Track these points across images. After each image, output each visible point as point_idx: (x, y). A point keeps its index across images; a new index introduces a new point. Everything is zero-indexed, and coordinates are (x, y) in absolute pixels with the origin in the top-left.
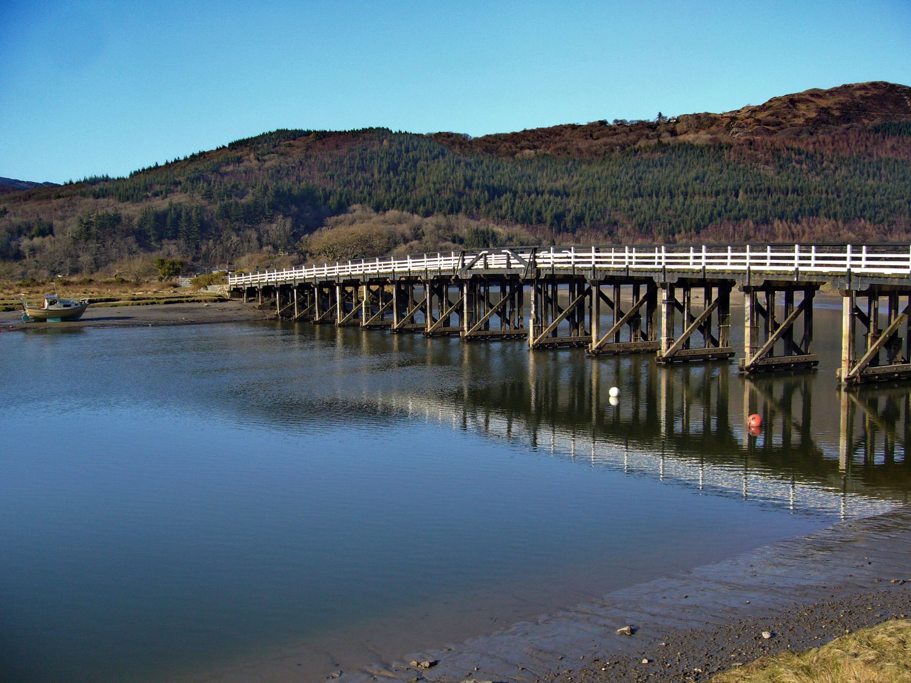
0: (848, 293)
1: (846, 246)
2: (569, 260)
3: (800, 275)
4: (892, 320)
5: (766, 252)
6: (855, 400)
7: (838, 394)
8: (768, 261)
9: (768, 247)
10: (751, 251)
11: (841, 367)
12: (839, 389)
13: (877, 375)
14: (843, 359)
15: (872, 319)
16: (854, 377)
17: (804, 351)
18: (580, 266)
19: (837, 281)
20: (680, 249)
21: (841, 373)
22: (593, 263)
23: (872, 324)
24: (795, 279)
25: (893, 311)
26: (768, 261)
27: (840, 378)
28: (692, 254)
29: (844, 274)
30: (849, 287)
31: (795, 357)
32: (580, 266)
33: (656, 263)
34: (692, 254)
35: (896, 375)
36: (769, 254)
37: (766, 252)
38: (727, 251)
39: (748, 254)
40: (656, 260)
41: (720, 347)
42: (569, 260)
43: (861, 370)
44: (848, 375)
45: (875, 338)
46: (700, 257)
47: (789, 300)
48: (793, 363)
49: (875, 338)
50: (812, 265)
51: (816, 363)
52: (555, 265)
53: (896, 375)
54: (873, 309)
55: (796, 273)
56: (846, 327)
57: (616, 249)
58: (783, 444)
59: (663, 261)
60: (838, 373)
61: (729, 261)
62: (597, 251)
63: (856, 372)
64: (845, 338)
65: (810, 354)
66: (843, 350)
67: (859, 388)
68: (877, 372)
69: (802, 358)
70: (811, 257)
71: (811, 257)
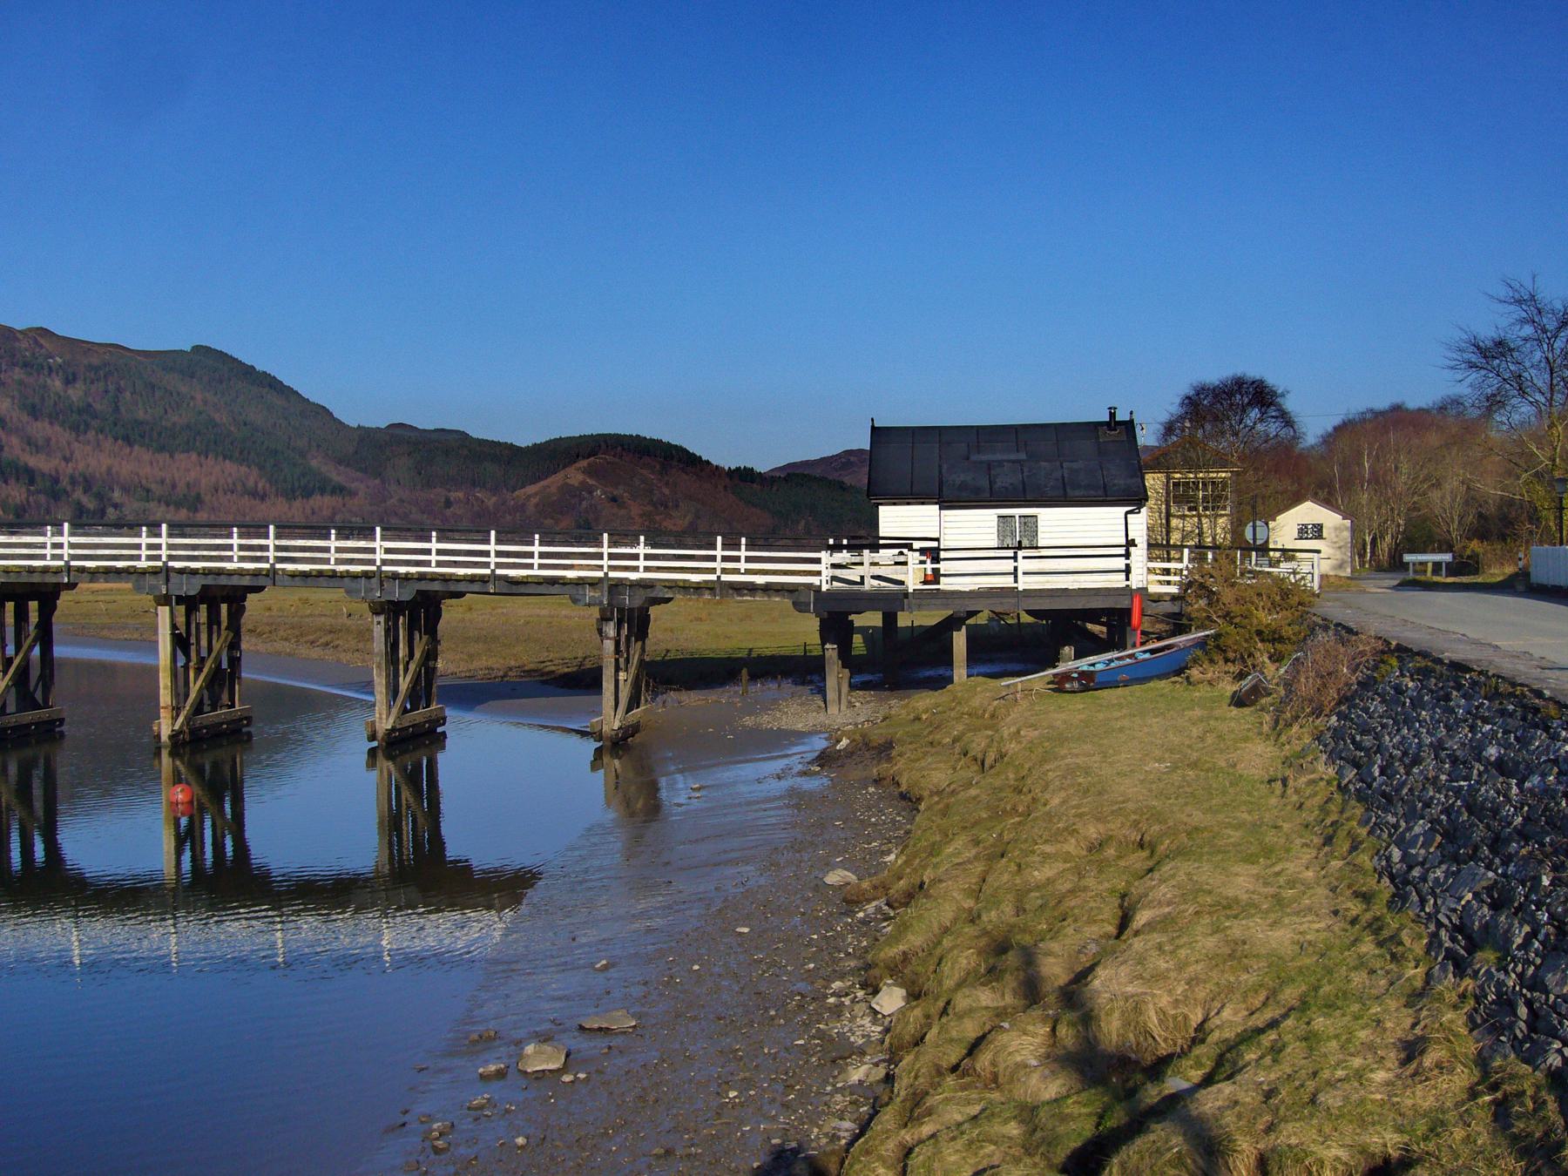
0: (165, 600)
1: (160, 526)
2: (325, 555)
3: (72, 573)
4: (214, 641)
5: (140, 536)
6: (182, 769)
7: (156, 762)
8: (641, 563)
9: (235, 530)
10: (499, 542)
11: (159, 718)
12: (158, 754)
13: (205, 727)
14: (162, 705)
15: (193, 640)
16: (180, 732)
17: (41, 702)
18: (290, 567)
19: (145, 581)
20: (558, 538)
21: (159, 728)
22: (164, 559)
23: (193, 648)
24: (66, 580)
25: (215, 627)
26: (641, 563)
27: (159, 736)
28: (144, 540)
29: (158, 570)
30: (167, 590)
31: (29, 716)
32: (290, 567)
33: (641, 569)
34: (144, 540)
35: (225, 726)
36: (235, 541)
37: (140, 536)
38: (487, 542)
39: (537, 548)
40: (48, 551)
41: (237, 708)
42: (325, 555)
43: (188, 719)
44: (173, 731)
45: (199, 670)
46: (158, 547)
47: (21, 616)
48: (33, 724)
49: (199, 670)
50: (536, 566)
51: (62, 721)
52: (73, 563)
53: (225, 726)
54: (193, 626)
55: (164, 572)
56: (165, 654)
57: (503, 536)
58: (22, 865)
59: (164, 553)
60: (155, 728)
61: (236, 553)
62: (612, 544)
63: (182, 724)
64: (165, 671)
65: (52, 707)
66: (162, 691)
67: (187, 749)
68: (205, 723)
69: (43, 714)
70: (232, 545)
71: (232, 545)
